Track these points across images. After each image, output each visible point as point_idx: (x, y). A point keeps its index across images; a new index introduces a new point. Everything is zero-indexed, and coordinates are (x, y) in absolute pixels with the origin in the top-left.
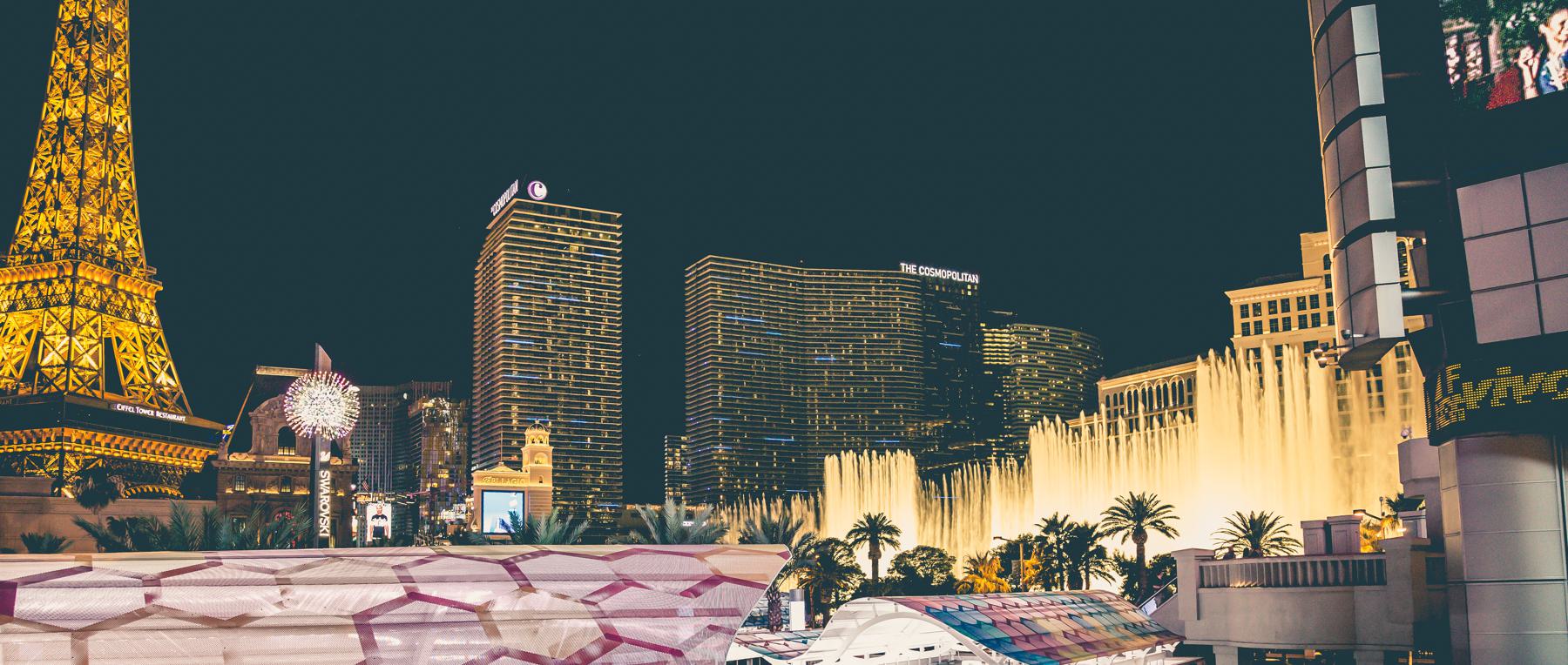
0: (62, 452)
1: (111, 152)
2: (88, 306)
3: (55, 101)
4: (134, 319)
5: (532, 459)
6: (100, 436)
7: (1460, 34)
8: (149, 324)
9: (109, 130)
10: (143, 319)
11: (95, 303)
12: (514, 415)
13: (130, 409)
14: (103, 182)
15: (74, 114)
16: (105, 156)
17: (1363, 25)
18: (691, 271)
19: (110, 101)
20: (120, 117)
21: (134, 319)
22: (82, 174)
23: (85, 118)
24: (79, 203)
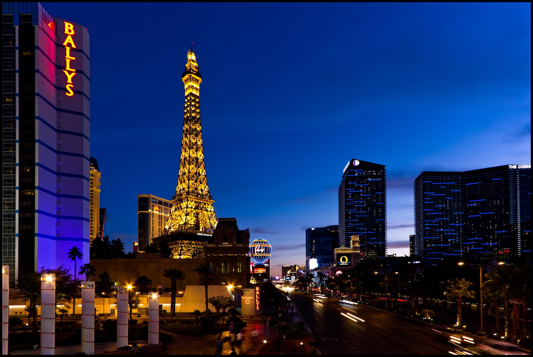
0: (182, 247)
1: (198, 166)
2: (191, 208)
3: (183, 153)
4: (207, 210)
5: (353, 245)
6: (193, 242)
7: (450, 200)
8: (211, 211)
9: (197, 159)
10: (209, 210)
11: (194, 207)
12: (107, 307)
13: (202, 235)
14: (196, 173)
15: (187, 156)
16: (196, 166)
17: (450, 352)
18: (240, 230)
19: (197, 151)
20: (200, 155)
21: (207, 210)
22: (189, 172)
23: (190, 156)
24: (189, 180)
